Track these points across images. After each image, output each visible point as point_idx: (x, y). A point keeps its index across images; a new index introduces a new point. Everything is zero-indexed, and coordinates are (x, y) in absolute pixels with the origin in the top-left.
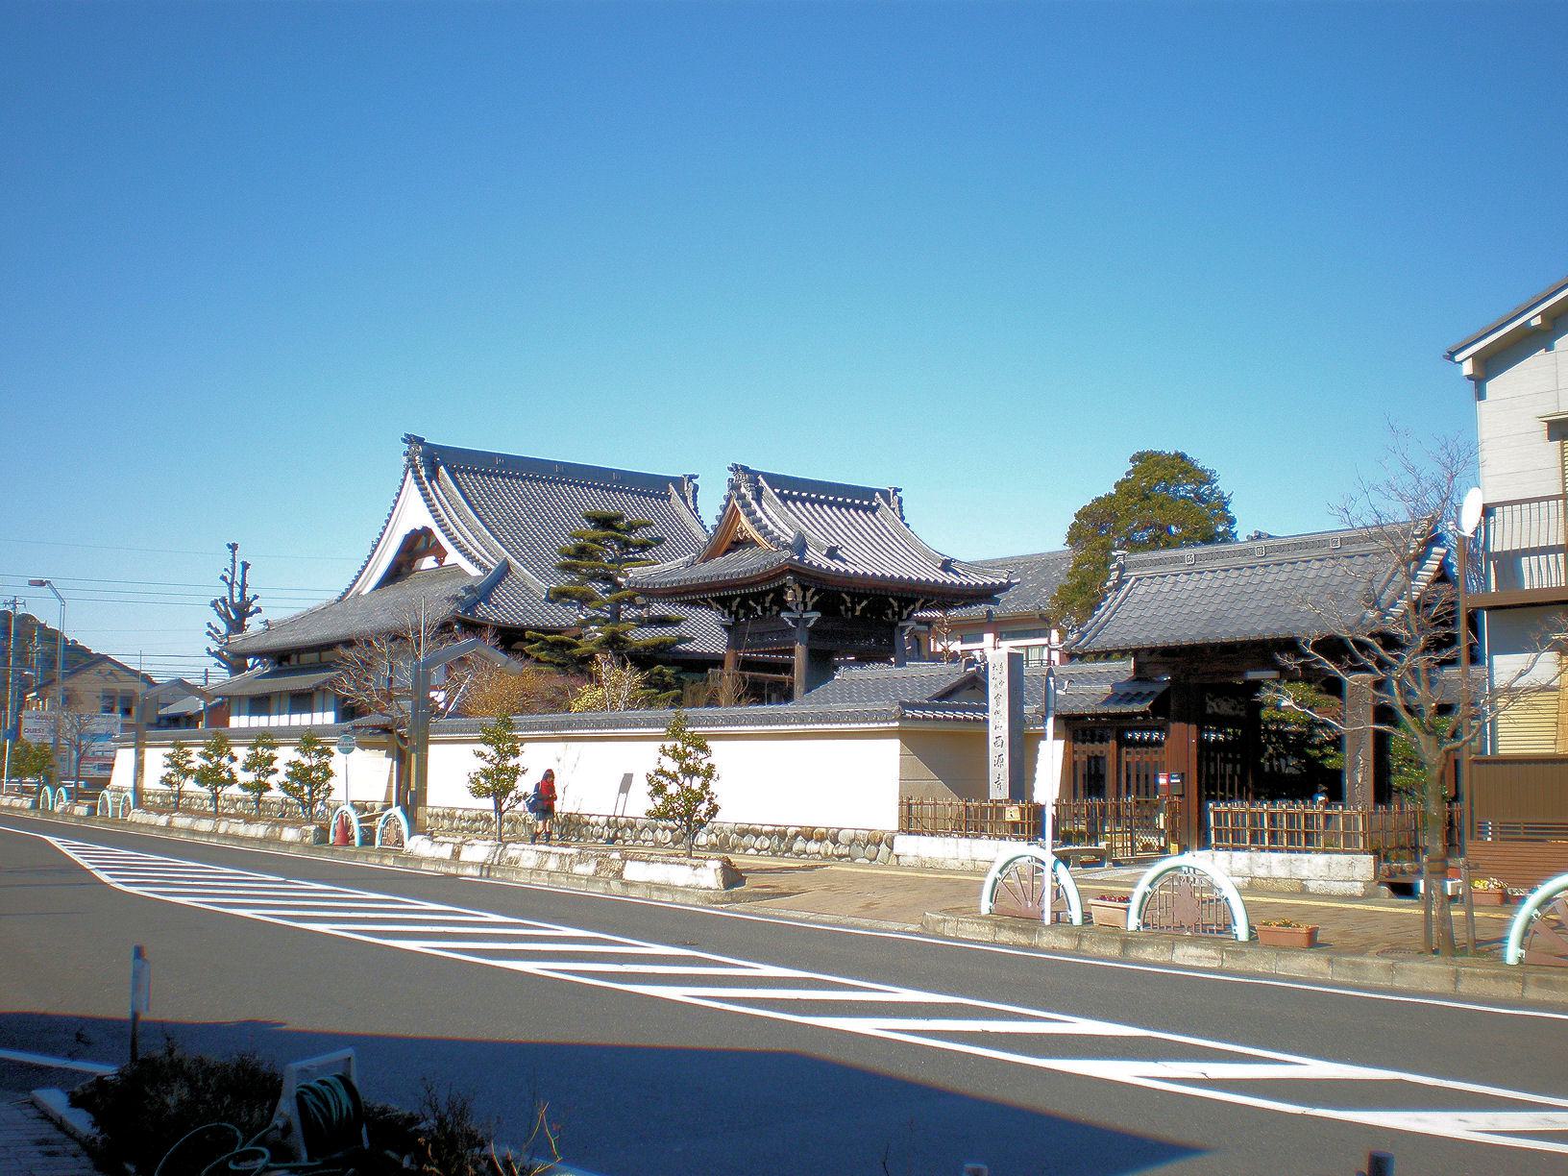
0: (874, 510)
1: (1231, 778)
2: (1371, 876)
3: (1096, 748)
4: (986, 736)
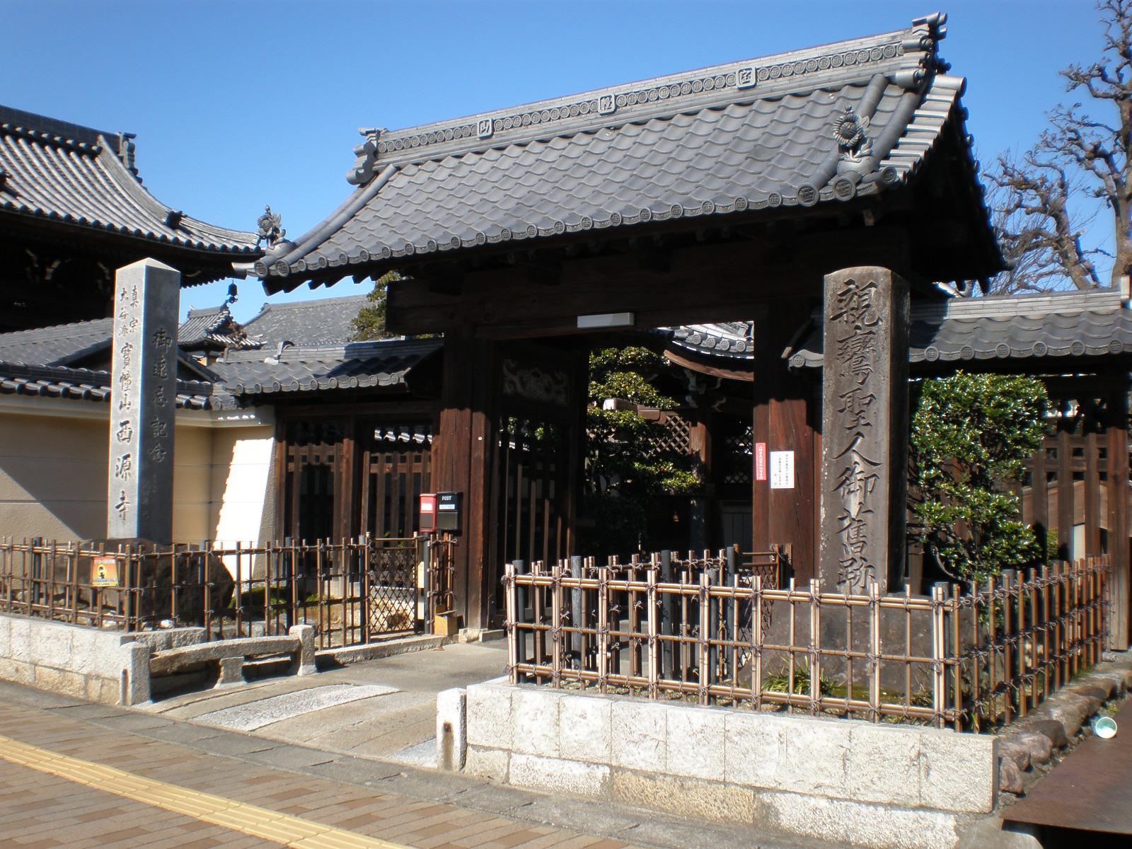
0: (93, 156)
1: (540, 503)
2: (981, 798)
3: (319, 451)
4: (105, 427)
